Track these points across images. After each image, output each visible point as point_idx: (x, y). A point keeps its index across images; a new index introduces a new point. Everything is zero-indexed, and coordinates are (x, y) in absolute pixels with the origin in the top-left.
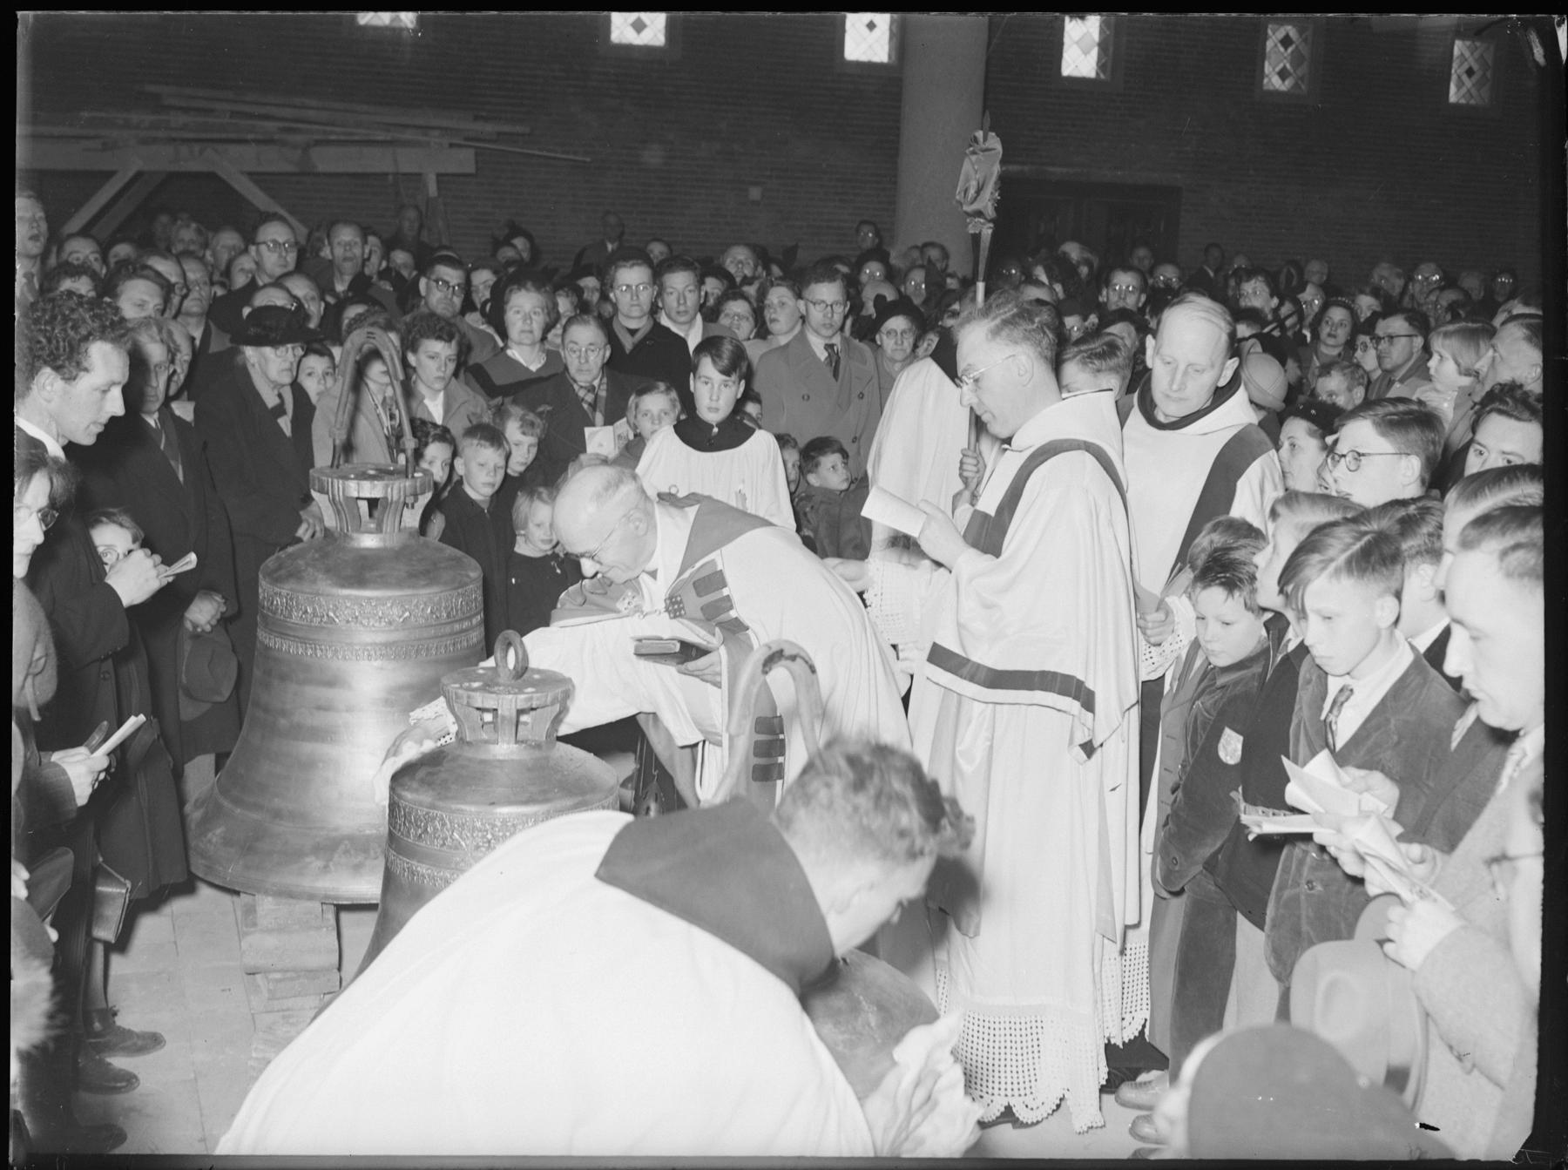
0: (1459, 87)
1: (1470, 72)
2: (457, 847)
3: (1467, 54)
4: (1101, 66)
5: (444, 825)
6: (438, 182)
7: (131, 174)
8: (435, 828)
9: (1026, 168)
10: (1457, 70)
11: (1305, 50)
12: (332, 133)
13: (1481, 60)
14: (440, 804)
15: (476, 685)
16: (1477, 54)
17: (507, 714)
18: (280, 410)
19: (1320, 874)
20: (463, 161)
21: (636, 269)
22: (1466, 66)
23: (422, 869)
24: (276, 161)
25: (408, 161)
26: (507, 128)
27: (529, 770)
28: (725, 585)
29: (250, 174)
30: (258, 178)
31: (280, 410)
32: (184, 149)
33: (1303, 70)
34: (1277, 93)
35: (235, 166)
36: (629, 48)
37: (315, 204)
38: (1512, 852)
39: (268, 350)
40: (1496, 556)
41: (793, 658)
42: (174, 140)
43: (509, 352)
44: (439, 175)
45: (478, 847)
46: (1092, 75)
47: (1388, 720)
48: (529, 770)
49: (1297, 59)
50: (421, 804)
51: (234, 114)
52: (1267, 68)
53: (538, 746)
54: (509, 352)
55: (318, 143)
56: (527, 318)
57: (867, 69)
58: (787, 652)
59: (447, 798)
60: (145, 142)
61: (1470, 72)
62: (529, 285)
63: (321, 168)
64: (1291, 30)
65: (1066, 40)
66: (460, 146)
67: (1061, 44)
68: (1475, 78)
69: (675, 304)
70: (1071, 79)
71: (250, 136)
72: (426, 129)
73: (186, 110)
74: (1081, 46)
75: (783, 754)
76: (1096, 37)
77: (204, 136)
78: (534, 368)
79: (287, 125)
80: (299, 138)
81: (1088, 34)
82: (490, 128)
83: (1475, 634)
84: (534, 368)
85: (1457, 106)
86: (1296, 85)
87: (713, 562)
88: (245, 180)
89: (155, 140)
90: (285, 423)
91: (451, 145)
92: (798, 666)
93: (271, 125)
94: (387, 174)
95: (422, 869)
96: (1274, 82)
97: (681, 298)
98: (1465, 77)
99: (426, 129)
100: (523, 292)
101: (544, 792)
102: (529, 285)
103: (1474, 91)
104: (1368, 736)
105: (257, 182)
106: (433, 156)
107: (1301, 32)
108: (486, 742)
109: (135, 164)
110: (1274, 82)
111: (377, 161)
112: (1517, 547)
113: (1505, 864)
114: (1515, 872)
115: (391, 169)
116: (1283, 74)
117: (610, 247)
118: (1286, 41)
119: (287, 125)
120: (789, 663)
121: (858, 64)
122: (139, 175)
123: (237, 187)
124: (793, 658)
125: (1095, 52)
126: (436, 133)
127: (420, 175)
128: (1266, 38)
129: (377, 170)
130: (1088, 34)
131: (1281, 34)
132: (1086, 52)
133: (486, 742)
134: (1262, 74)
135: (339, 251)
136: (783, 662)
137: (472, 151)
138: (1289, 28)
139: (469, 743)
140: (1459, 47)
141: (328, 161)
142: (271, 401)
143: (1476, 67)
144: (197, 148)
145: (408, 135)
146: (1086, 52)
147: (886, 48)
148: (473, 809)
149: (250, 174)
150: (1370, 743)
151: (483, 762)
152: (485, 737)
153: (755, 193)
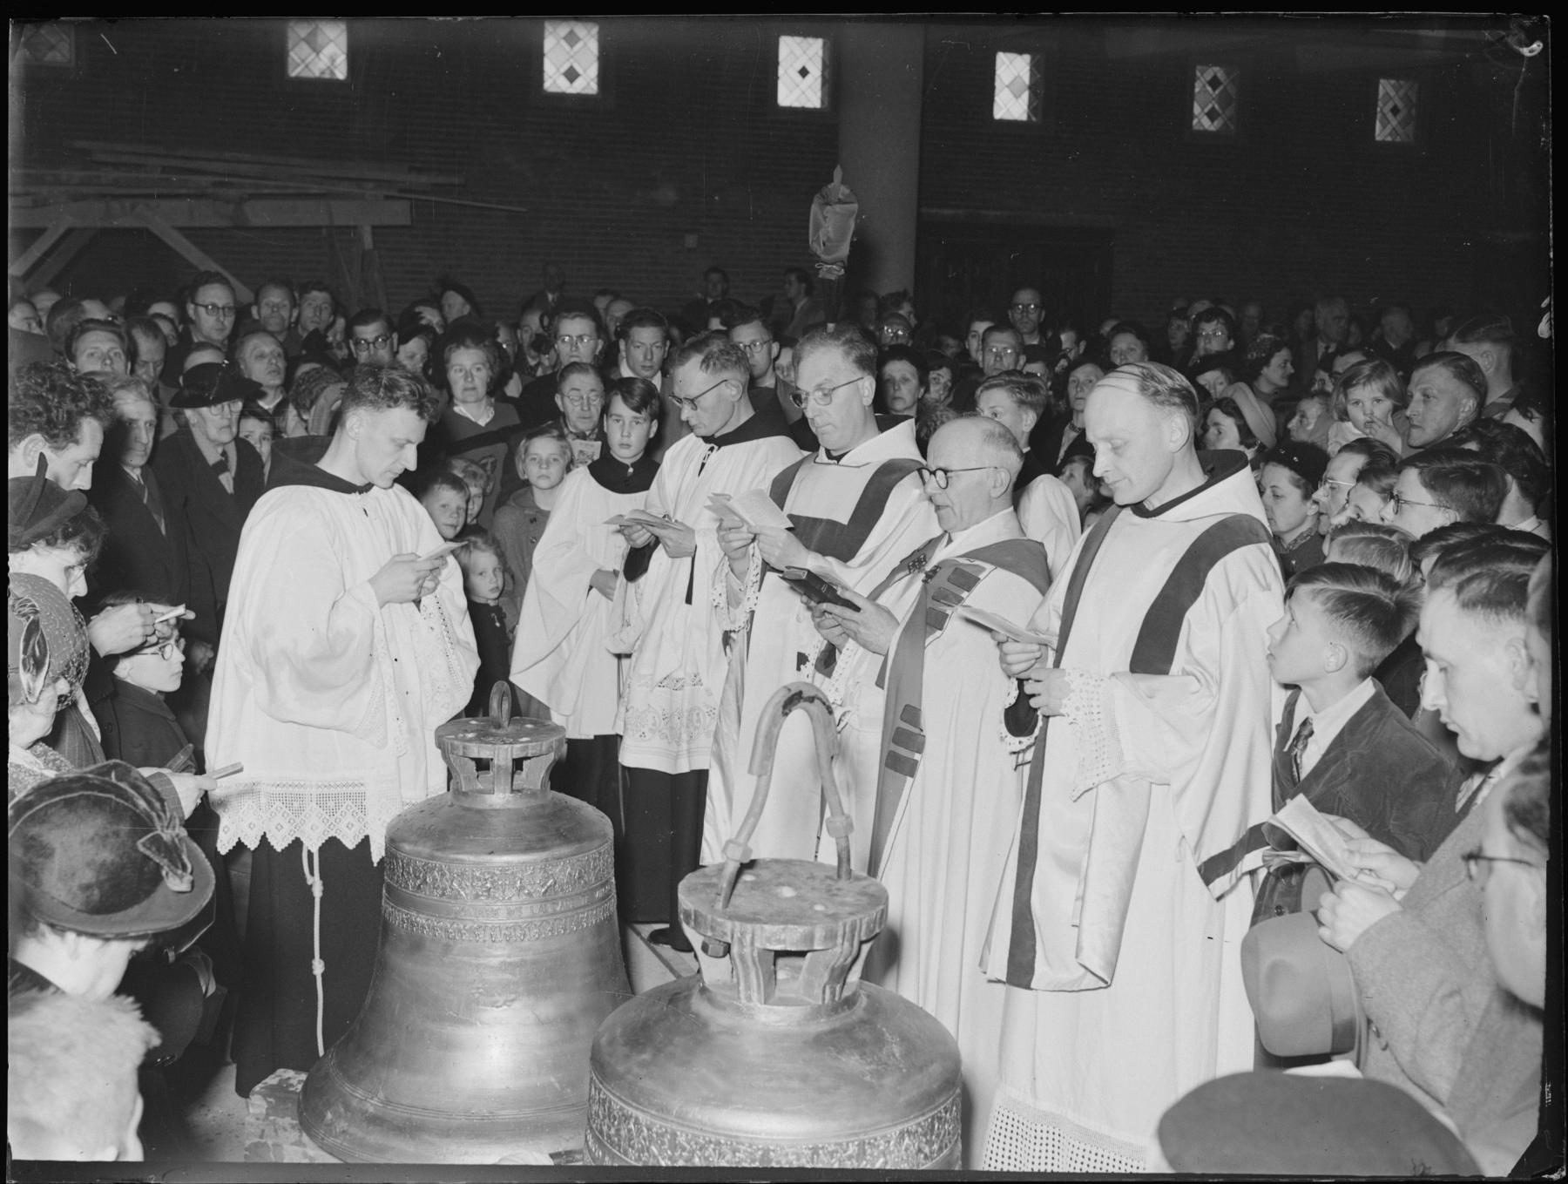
0: (1384, 127)
1: (1395, 111)
2: (457, 897)
3: (1392, 93)
4: (1032, 108)
5: (443, 875)
6: (374, 234)
7: (61, 231)
8: (435, 879)
9: (961, 212)
10: (1383, 108)
11: (1232, 90)
12: (266, 187)
13: (1406, 99)
14: (439, 854)
15: (470, 735)
16: (1401, 93)
17: (502, 763)
18: (222, 466)
19: (1288, 899)
20: (398, 213)
21: (578, 320)
22: (1390, 105)
23: (422, 919)
24: (208, 216)
25: (343, 214)
26: (441, 180)
27: (525, 818)
28: (969, 590)
29: (181, 229)
30: (189, 232)
31: (222, 466)
32: (115, 205)
33: (1230, 111)
34: (1205, 133)
35: (165, 221)
36: (562, 97)
37: (254, 259)
38: (1489, 852)
39: (204, 410)
40: (1453, 590)
41: (811, 699)
42: (104, 196)
43: (456, 409)
44: (374, 227)
45: (477, 896)
46: (1024, 117)
47: (1344, 753)
48: (525, 818)
49: (1224, 100)
50: (419, 855)
51: (164, 169)
52: (1197, 109)
53: (533, 794)
54: (456, 409)
55: (252, 197)
56: (468, 375)
57: (800, 115)
58: (805, 695)
59: (445, 849)
60: (76, 198)
61: (1395, 111)
62: (468, 342)
63: (256, 221)
64: (1221, 74)
65: (998, 84)
66: (393, 198)
67: (993, 88)
68: (1400, 117)
69: (641, 358)
70: (1001, 122)
71: (183, 191)
72: (359, 181)
73: (116, 166)
74: (1012, 86)
75: (920, 751)
76: (1026, 79)
77: (136, 191)
78: (482, 422)
79: (218, 179)
80: (232, 192)
81: (1018, 77)
82: (424, 179)
83: (1444, 665)
84: (482, 422)
85: (1383, 143)
86: (1225, 124)
87: (984, 569)
88: (176, 235)
89: (84, 197)
90: (227, 480)
91: (387, 198)
92: (816, 707)
93: (205, 180)
94: (319, 227)
95: (422, 919)
96: (1201, 122)
97: (648, 354)
98: (1390, 116)
99: (359, 181)
100: (462, 349)
101: (542, 840)
102: (468, 342)
103: (1399, 129)
104: (1327, 770)
105: (187, 237)
106: (368, 210)
107: (1228, 74)
108: (482, 792)
109: (69, 221)
110: (1201, 122)
111: (308, 214)
112: (1470, 580)
113: (1483, 863)
114: (1491, 870)
115: (326, 222)
116: (1212, 115)
117: (550, 297)
118: (1214, 83)
119: (218, 179)
120: (807, 704)
121: (792, 111)
122: (69, 232)
123: (170, 243)
124: (811, 699)
125: (1026, 96)
126: (371, 185)
127: (355, 227)
128: (1194, 79)
129: (311, 223)
130: (1018, 77)
131: (1209, 75)
132: (1017, 96)
133: (482, 792)
134: (1191, 116)
135: (265, 311)
136: (803, 704)
137: (406, 204)
138: (1216, 69)
139: (465, 794)
140: (1385, 87)
141: (261, 215)
142: (212, 457)
143: (1400, 105)
144: (128, 203)
145: (342, 188)
146: (1017, 96)
147: (819, 94)
148: (472, 858)
149: (181, 229)
150: (1328, 776)
151: (479, 812)
152: (480, 786)
153: (691, 241)
